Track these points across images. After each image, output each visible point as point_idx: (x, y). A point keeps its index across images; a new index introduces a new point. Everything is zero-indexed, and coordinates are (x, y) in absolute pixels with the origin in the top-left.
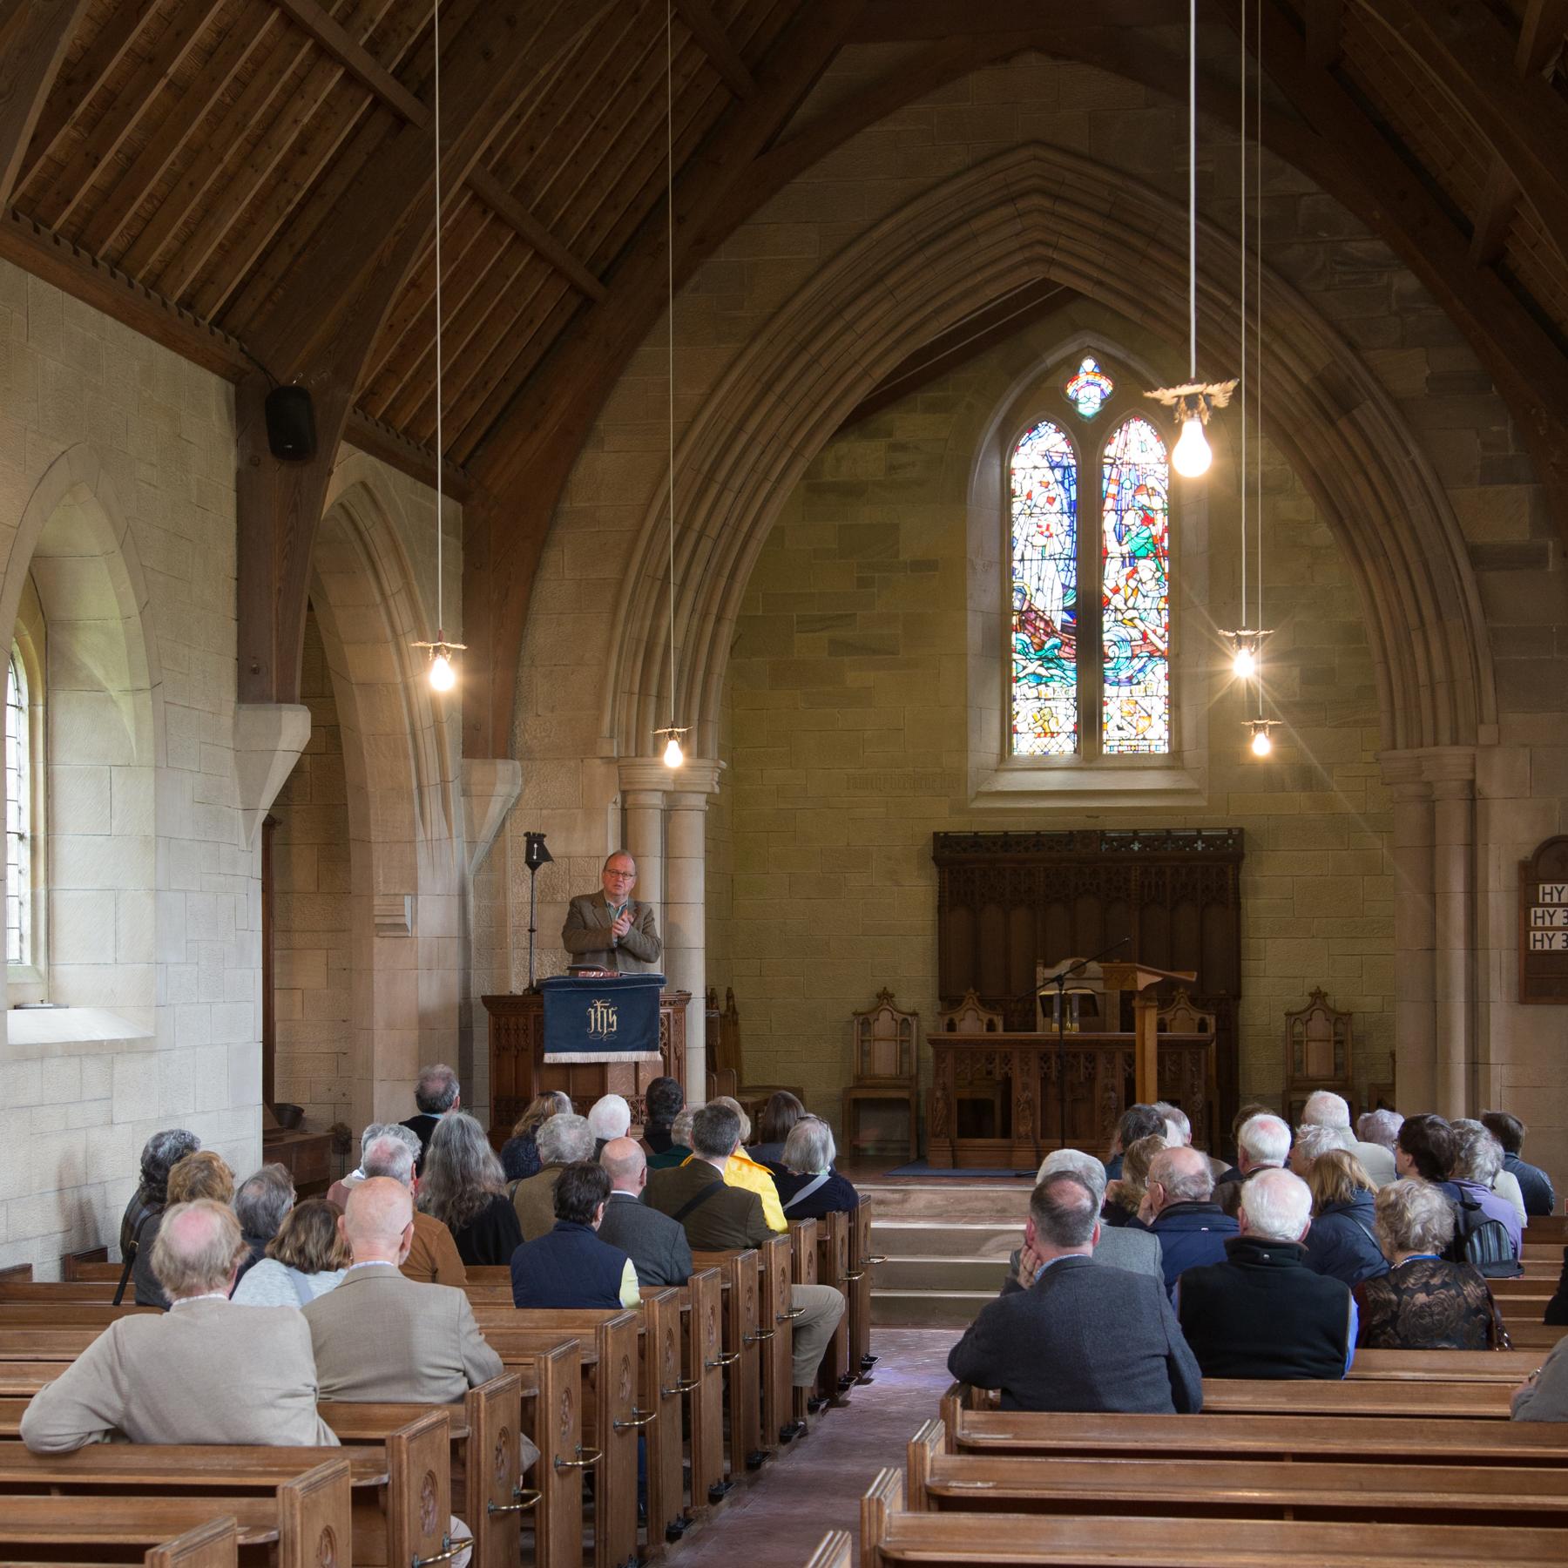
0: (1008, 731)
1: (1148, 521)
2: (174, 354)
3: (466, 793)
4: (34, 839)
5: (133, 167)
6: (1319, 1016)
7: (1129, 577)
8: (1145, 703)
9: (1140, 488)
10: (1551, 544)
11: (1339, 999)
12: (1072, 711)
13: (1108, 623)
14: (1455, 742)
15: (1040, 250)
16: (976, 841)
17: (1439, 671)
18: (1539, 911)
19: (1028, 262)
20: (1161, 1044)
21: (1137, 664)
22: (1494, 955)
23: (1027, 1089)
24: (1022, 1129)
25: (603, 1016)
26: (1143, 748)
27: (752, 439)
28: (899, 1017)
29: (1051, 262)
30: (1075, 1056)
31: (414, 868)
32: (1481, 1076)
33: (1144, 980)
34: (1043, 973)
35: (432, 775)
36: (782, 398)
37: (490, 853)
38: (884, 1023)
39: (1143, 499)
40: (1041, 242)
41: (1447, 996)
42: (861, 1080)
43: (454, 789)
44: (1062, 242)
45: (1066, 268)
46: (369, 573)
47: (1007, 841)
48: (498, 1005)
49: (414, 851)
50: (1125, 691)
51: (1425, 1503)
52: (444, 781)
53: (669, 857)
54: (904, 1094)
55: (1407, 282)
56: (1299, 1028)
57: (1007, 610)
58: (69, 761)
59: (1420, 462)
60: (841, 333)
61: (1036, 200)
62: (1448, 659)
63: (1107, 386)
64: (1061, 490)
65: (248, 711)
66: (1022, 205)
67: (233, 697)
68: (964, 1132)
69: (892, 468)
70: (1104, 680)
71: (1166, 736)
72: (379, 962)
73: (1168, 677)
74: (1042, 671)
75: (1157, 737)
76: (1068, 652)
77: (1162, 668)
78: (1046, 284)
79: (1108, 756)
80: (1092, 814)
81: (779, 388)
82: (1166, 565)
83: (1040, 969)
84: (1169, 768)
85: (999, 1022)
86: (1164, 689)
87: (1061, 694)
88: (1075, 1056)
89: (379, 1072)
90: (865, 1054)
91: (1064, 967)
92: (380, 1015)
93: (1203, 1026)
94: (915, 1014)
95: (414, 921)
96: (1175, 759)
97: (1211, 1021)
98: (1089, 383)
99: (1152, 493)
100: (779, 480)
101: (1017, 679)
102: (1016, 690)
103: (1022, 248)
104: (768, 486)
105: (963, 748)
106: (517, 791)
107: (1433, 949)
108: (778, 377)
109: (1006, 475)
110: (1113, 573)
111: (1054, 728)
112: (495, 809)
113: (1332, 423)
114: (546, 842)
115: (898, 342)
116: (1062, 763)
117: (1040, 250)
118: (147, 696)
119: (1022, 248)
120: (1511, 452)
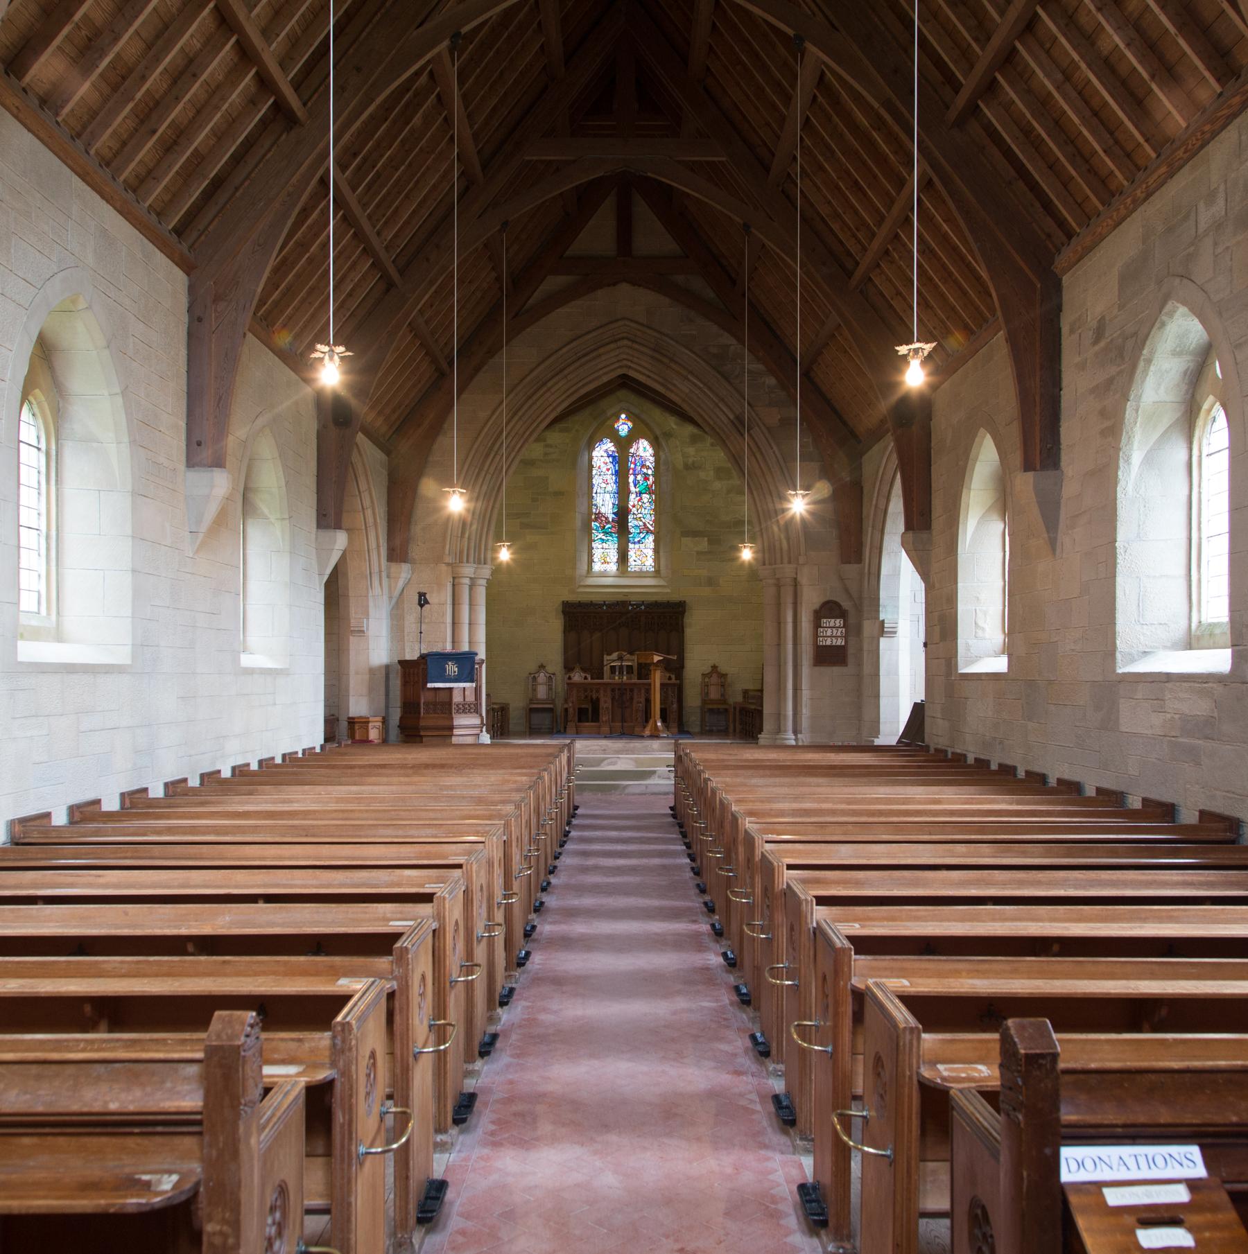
1: (646, 479)
3: (388, 577)
6: (715, 675)
7: (639, 500)
8: (645, 551)
11: (723, 668)
12: (616, 554)
13: (630, 517)
14: (789, 562)
15: (625, 362)
16: (580, 605)
18: (822, 630)
19: (621, 367)
21: (642, 535)
23: (605, 703)
24: (604, 719)
25: (452, 668)
26: (644, 569)
28: (548, 675)
30: (626, 689)
31: (368, 606)
32: (798, 694)
33: (656, 658)
34: (606, 657)
35: (375, 569)
36: (520, 418)
37: (397, 603)
38: (542, 677)
39: (645, 470)
41: (785, 663)
42: (531, 701)
43: (384, 575)
44: (635, 360)
45: (636, 371)
48: (403, 663)
49: (368, 600)
50: (637, 546)
51: (129, 992)
52: (380, 572)
53: (472, 604)
54: (551, 706)
56: (707, 680)
57: (590, 513)
59: (777, 452)
60: (545, 393)
61: (625, 342)
63: (630, 424)
65: (323, 533)
66: (620, 343)
67: (315, 526)
68: (580, 720)
69: (546, 454)
70: (629, 541)
71: (653, 564)
73: (654, 541)
75: (649, 563)
76: (614, 530)
77: (651, 538)
80: (626, 594)
81: (520, 413)
83: (605, 656)
84: (654, 577)
85: (673, 677)
86: (652, 545)
87: (611, 547)
88: (626, 689)
89: (351, 692)
90: (534, 690)
91: (615, 655)
92: (352, 669)
94: (554, 674)
95: (368, 629)
96: (657, 573)
98: (623, 424)
99: (648, 468)
101: (594, 541)
102: (594, 545)
103: (618, 361)
105: (574, 568)
106: (409, 576)
108: (519, 409)
109: (591, 459)
110: (633, 499)
111: (609, 560)
112: (401, 584)
114: (427, 596)
115: (568, 396)
116: (612, 574)
117: (625, 362)
118: (288, 521)
119: (618, 361)
120: (811, 449)
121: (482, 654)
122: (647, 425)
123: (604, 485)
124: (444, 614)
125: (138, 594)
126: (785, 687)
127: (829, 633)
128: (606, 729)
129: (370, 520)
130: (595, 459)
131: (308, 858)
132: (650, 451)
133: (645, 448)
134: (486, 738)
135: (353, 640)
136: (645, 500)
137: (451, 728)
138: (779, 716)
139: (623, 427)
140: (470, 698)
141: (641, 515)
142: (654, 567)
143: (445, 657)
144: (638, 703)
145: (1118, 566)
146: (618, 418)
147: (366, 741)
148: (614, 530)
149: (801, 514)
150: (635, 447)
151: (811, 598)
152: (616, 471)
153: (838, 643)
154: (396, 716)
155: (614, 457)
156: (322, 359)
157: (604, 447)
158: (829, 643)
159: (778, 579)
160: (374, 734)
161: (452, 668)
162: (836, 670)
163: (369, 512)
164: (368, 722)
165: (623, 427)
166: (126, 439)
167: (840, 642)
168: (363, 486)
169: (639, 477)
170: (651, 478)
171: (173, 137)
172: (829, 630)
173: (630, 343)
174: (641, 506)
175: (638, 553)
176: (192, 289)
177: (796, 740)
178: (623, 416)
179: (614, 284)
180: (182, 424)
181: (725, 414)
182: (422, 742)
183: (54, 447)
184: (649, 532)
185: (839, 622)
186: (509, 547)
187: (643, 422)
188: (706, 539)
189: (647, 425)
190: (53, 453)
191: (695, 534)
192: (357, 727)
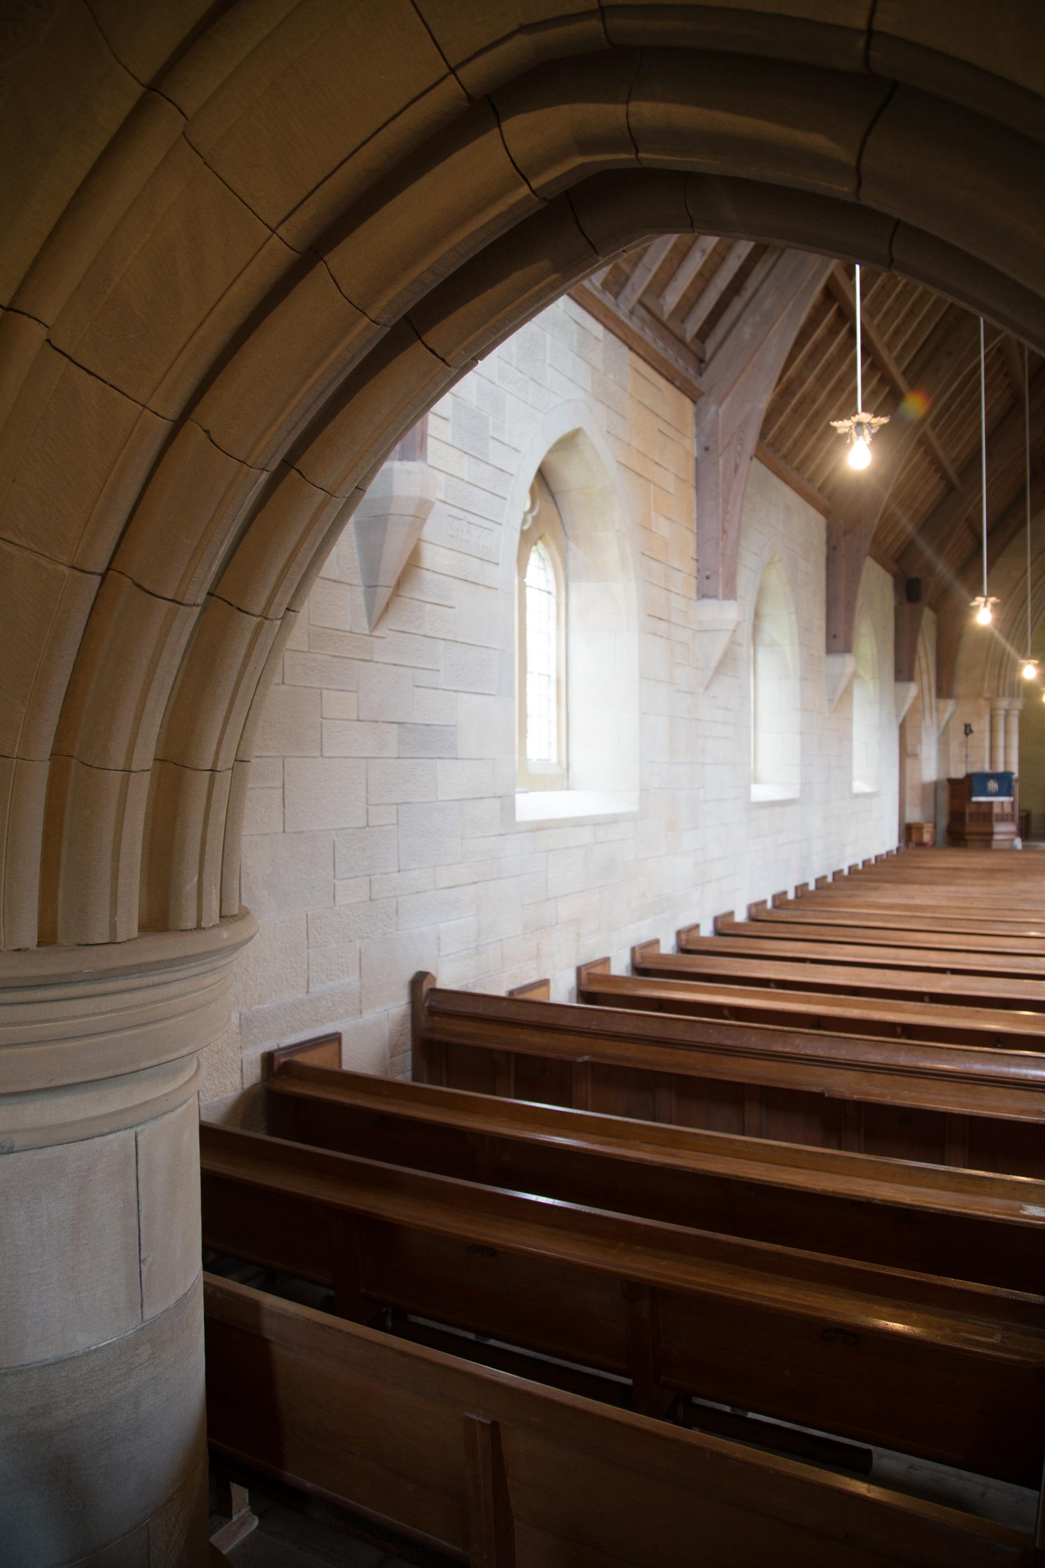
25: (993, 785)
48: (952, 782)
53: (1007, 732)
112: (947, 715)
121: (1016, 775)
125: (804, 749)
131: (961, 944)
134: (1018, 843)
137: (991, 834)
143: (986, 777)
147: (921, 844)
154: (943, 822)
156: (978, 606)
160: (927, 838)
161: (993, 785)
180: (823, 624)
192: (913, 831)
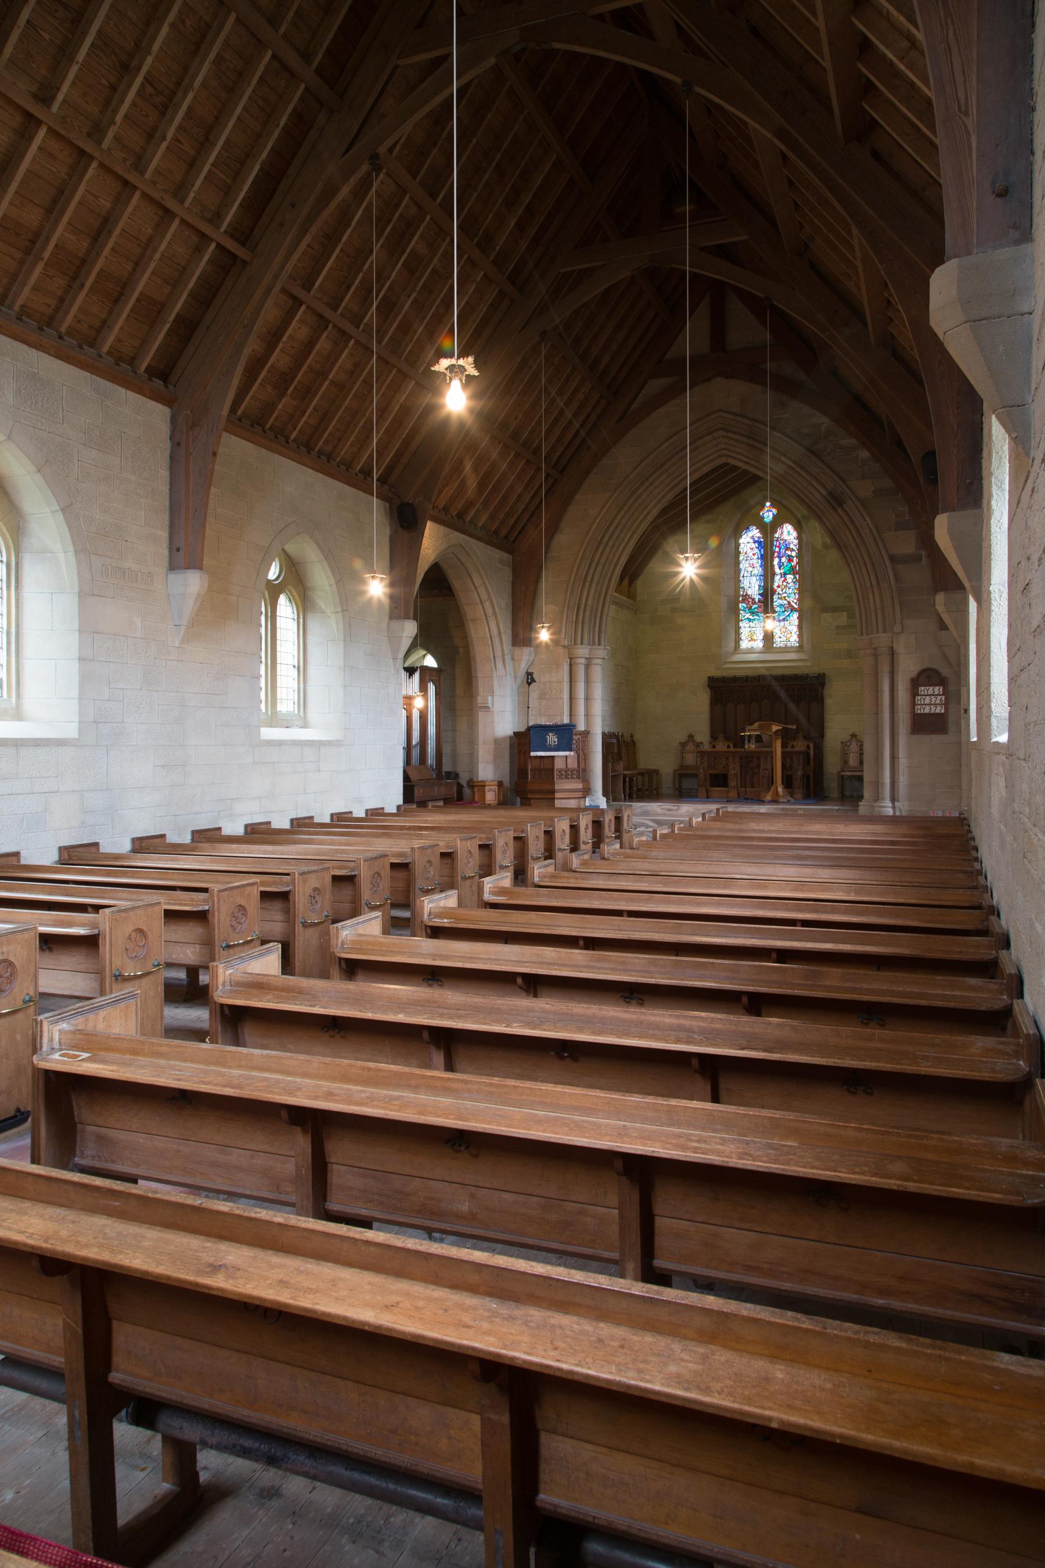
0: (738, 639)
1: (790, 560)
2: (356, 490)
3: (513, 659)
4: (299, 667)
5: (325, 418)
6: (691, 744)
7: (784, 581)
8: (790, 628)
9: (787, 549)
10: (924, 553)
13: (775, 597)
14: (885, 631)
15: (724, 452)
16: (723, 680)
17: (878, 605)
18: (919, 698)
19: (720, 456)
20: (783, 753)
21: (787, 613)
22: (900, 715)
25: (552, 739)
26: (789, 645)
27: (616, 527)
29: (729, 456)
31: (493, 685)
33: (775, 728)
35: (499, 653)
36: (626, 512)
39: (789, 553)
40: (726, 449)
41: (882, 731)
42: (682, 767)
43: (508, 658)
45: (734, 458)
46: (468, 579)
47: (735, 679)
50: (782, 623)
52: (503, 655)
55: (864, 454)
58: (312, 639)
59: (870, 523)
61: (721, 433)
62: (882, 600)
63: (775, 511)
64: (757, 551)
72: (480, 721)
73: (798, 618)
74: (751, 617)
76: (760, 610)
77: (796, 615)
78: (726, 464)
79: (776, 648)
81: (625, 509)
82: (797, 576)
85: (732, 746)
86: (796, 622)
89: (480, 759)
92: (481, 739)
93: (808, 747)
95: (493, 705)
96: (800, 648)
97: (812, 745)
98: (768, 511)
99: (792, 550)
100: (627, 543)
102: (741, 624)
104: (623, 545)
106: (532, 659)
107: (877, 714)
109: (738, 545)
113: (836, 510)
115: (671, 489)
116: (757, 650)
117: (724, 452)
118: (341, 614)
122: (790, 511)
123: (750, 569)
124: (561, 691)
126: (882, 755)
127: (927, 701)
128: (733, 794)
129: (489, 611)
130: (742, 546)
132: (795, 534)
133: (789, 532)
135: (481, 714)
136: (790, 581)
137: (553, 792)
138: (877, 784)
139: (768, 514)
140: (573, 764)
141: (785, 595)
142: (799, 642)
144: (764, 770)
145: (993, 614)
146: (763, 506)
148: (760, 610)
149: (697, 574)
150: (779, 531)
151: (908, 666)
152: (762, 556)
153: (938, 711)
155: (759, 543)
157: (750, 534)
158: (927, 710)
159: (875, 648)
162: (936, 738)
163: (487, 605)
164: (485, 786)
165: (768, 514)
166: (71, 549)
167: (940, 710)
168: (478, 582)
169: (784, 559)
170: (795, 560)
171: (118, 289)
172: (928, 698)
173: (724, 433)
174: (786, 586)
175: (784, 630)
176: (173, 420)
177: (894, 807)
178: (768, 504)
179: (708, 380)
181: (817, 490)
182: (530, 805)
183: (13, 559)
184: (793, 610)
185: (938, 690)
186: (549, 628)
187: (786, 507)
188: (845, 614)
189: (790, 511)
190: (13, 564)
191: (835, 609)
